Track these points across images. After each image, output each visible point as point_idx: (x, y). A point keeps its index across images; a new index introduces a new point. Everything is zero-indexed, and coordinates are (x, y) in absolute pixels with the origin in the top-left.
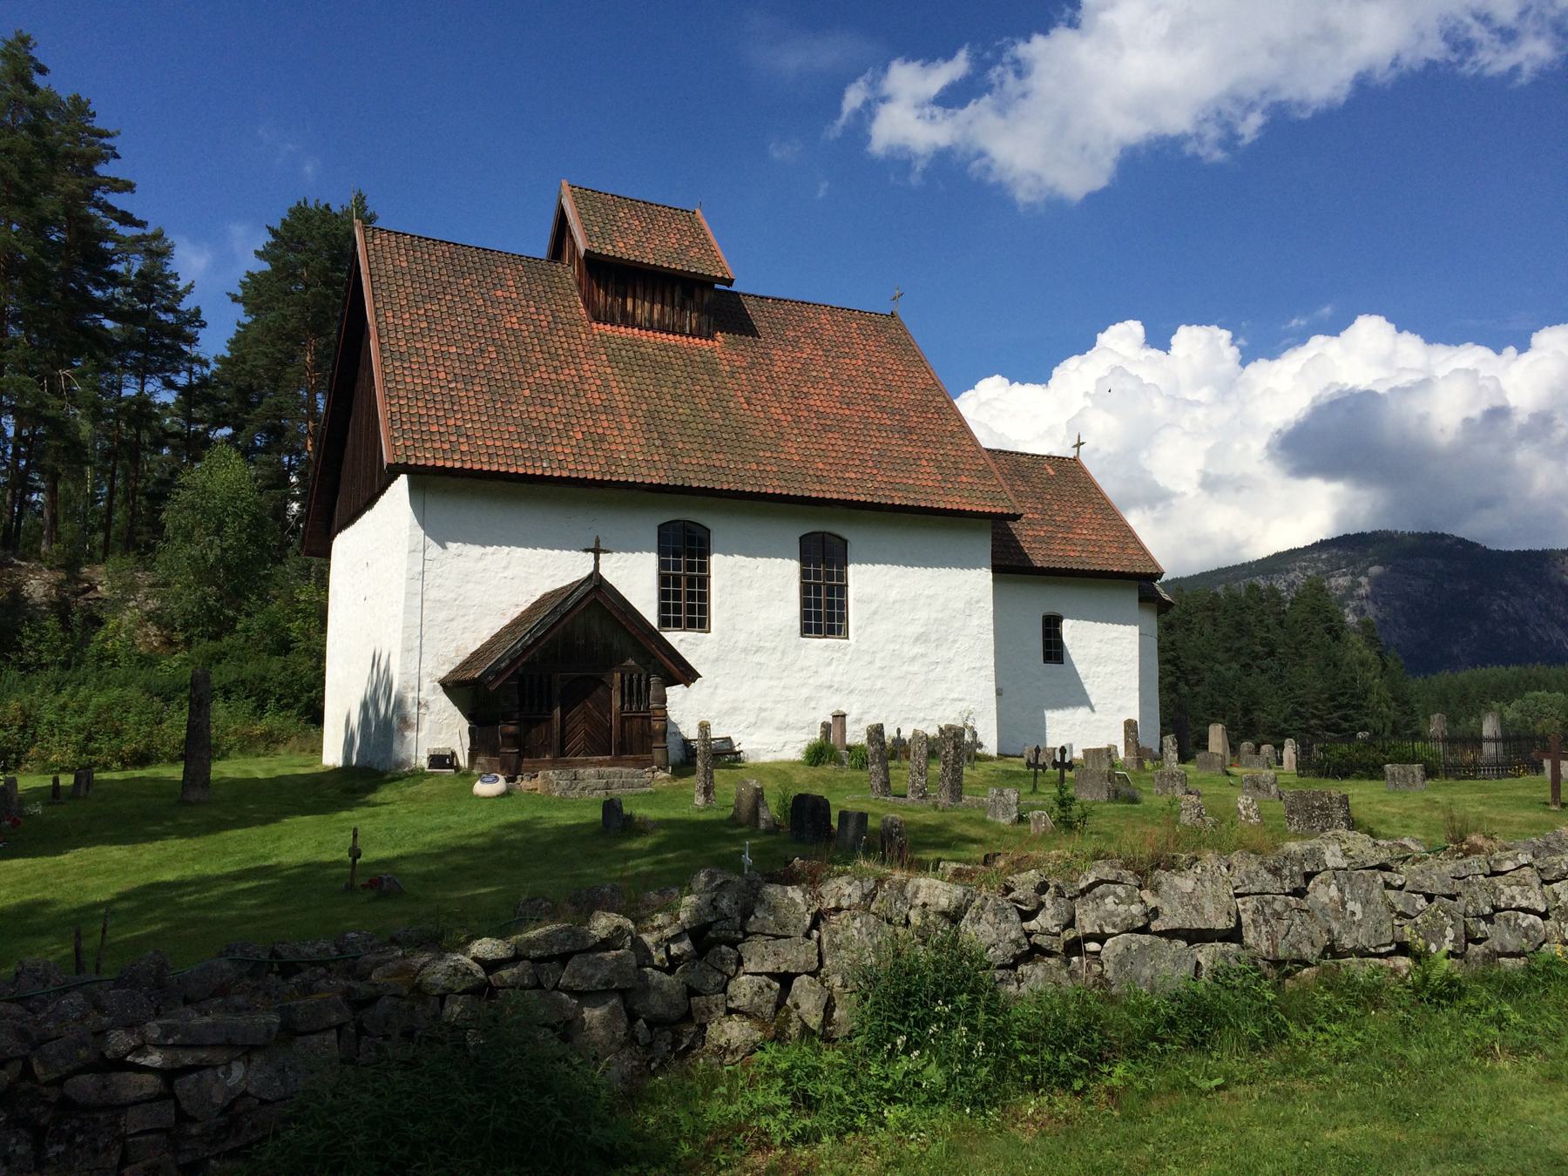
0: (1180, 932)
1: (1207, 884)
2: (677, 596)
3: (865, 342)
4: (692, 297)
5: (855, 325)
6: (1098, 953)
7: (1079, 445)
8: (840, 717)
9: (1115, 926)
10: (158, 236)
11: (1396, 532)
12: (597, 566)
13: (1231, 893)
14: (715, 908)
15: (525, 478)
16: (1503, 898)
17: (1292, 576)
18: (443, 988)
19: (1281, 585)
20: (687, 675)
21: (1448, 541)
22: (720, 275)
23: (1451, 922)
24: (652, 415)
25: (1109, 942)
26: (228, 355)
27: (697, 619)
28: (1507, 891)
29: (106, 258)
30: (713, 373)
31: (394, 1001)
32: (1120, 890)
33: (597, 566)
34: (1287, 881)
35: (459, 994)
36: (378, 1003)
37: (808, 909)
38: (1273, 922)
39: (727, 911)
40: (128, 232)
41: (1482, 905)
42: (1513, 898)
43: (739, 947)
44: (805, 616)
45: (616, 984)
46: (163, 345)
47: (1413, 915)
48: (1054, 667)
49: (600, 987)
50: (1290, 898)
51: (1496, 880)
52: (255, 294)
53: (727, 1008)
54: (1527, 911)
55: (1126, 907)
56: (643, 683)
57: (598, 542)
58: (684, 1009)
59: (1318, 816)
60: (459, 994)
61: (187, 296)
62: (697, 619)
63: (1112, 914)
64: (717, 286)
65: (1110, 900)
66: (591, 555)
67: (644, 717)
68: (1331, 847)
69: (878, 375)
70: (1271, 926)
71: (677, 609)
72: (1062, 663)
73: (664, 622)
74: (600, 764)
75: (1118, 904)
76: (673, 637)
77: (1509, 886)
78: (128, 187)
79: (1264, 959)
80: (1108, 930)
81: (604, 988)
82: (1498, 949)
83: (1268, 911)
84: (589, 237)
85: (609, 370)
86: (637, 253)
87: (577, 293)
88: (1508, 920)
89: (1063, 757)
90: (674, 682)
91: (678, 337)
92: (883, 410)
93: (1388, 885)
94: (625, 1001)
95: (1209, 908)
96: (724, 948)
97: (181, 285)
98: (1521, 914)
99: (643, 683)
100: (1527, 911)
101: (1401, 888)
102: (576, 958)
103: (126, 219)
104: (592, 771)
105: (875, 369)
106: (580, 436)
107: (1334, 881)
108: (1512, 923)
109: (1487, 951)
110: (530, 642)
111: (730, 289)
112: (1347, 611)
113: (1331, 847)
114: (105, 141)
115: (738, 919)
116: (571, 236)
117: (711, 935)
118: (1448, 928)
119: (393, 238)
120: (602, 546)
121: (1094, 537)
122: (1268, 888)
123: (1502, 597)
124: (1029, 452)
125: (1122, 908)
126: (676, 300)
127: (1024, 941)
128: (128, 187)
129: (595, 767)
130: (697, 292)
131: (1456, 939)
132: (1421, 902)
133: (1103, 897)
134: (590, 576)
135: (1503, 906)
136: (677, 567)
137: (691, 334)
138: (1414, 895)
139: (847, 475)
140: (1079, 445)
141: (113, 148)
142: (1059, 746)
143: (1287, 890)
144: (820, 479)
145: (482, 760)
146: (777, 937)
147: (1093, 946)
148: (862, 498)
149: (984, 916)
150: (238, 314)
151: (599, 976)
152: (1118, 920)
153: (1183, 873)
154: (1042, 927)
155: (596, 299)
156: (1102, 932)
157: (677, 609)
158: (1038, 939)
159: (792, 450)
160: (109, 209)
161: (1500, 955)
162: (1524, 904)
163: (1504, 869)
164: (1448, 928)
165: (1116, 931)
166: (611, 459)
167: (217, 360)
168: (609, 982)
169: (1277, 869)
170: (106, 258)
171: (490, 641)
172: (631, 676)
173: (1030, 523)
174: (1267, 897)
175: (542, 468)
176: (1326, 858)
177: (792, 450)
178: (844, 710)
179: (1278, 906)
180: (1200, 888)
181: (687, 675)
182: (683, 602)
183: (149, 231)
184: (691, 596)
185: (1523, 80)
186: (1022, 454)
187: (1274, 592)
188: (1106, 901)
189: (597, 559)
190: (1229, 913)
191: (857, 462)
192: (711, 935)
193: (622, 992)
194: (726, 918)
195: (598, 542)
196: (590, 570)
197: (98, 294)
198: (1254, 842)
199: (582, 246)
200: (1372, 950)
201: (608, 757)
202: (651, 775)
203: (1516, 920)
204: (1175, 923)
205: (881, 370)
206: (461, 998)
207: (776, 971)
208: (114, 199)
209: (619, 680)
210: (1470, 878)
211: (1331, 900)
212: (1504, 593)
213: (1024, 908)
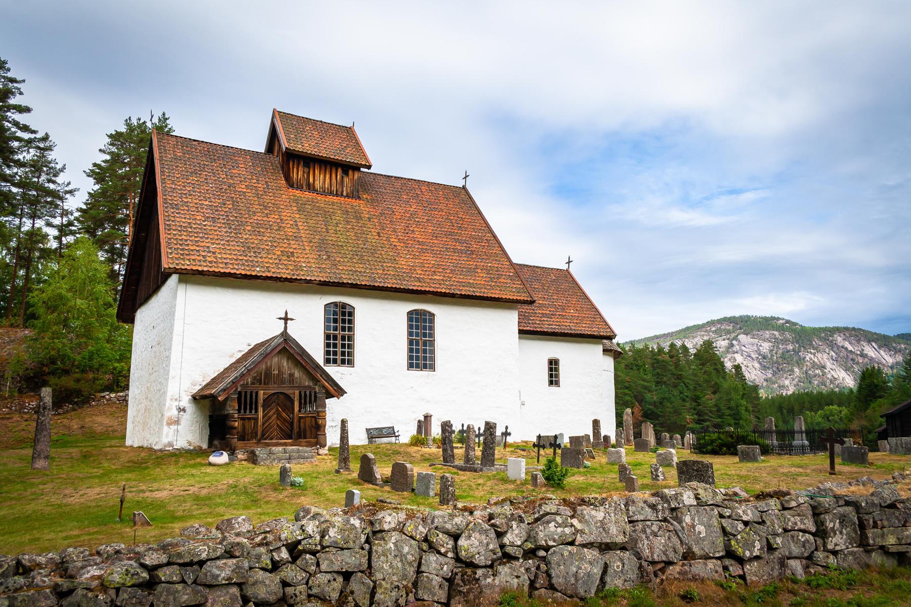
0: (595, 545)
1: (612, 515)
2: (335, 346)
3: (447, 202)
5: (441, 193)
6: (545, 557)
7: (569, 262)
8: (427, 417)
9: (554, 541)
10: (46, 138)
11: (752, 316)
12: (286, 328)
13: (626, 520)
14: (303, 531)
15: (245, 277)
16: (790, 524)
17: (696, 339)
18: (118, 583)
19: (689, 345)
20: (339, 392)
21: (781, 321)
22: (363, 163)
23: (758, 538)
24: (323, 241)
25: (552, 550)
26: (84, 207)
27: (347, 360)
28: (792, 519)
29: (13, 151)
30: (359, 218)
31: (85, 592)
32: (558, 518)
33: (286, 328)
34: (660, 513)
35: (129, 587)
36: (74, 594)
37: (363, 531)
38: (651, 537)
39: (311, 533)
40: (26, 136)
41: (777, 528)
42: (796, 524)
43: (317, 555)
44: (410, 358)
45: (235, 580)
46: (46, 202)
47: (736, 533)
48: (554, 388)
49: (224, 582)
50: (663, 523)
51: (786, 512)
52: (98, 174)
53: (308, 594)
54: (804, 531)
55: (562, 529)
56: (313, 397)
57: (286, 313)
58: (280, 595)
59: (695, 476)
60: (129, 587)
61: (62, 173)
62: (347, 360)
63: (553, 533)
64: (362, 169)
65: (553, 524)
66: (289, 322)
68: (687, 492)
69: (454, 221)
70: (650, 540)
71: (335, 353)
72: (432, 368)
73: (327, 361)
74: (285, 444)
75: (557, 527)
76: (331, 370)
77: (793, 516)
78: (27, 110)
79: (646, 561)
80: (551, 543)
81: (227, 582)
82: (787, 554)
83: (648, 531)
84: (288, 140)
85: (298, 216)
86: (316, 150)
87: (281, 172)
88: (792, 537)
89: (555, 441)
90: (330, 396)
91: (339, 198)
92: (457, 240)
93: (721, 516)
94: (241, 590)
95: (614, 530)
96: (308, 556)
97: (59, 167)
98: (801, 534)
99: (313, 397)
100: (804, 531)
101: (729, 517)
102: (208, 563)
103: (25, 128)
104: (280, 448)
105: (452, 218)
106: (279, 253)
107: (689, 513)
108: (795, 539)
109: (780, 556)
110: (245, 372)
111: (369, 171)
112: (726, 360)
113: (687, 492)
114: (15, 85)
115: (318, 538)
116: (278, 141)
117: (300, 547)
118: (757, 542)
119: (334, 188)
120: (283, 316)
121: (577, 315)
122: (649, 518)
123: (811, 353)
124: (540, 266)
125: (559, 530)
126: (338, 177)
127: (499, 550)
128: (27, 110)
129: (282, 446)
130: (350, 172)
131: (762, 548)
132: (740, 526)
133: (548, 522)
134: (282, 334)
135: (790, 528)
137: (348, 196)
138: (736, 522)
139: (435, 277)
140: (569, 262)
141: (19, 89)
142: (479, 425)
143: (660, 518)
144: (419, 280)
145: (216, 442)
146: (342, 549)
147: (542, 553)
148: (443, 291)
149: (473, 535)
150: (91, 185)
151: (223, 575)
152: (556, 537)
153: (598, 508)
154: (510, 542)
155: (291, 175)
156: (547, 545)
157: (335, 353)
158: (509, 550)
159: (404, 262)
160: (16, 124)
161: (789, 558)
162: (802, 527)
163: (791, 506)
164: (757, 542)
165: (555, 544)
166: (298, 268)
167: (78, 210)
168: (229, 579)
169: (654, 505)
170: (13, 151)
171: (223, 372)
172: (305, 392)
173: (541, 306)
174: (648, 523)
175: (257, 271)
176: (684, 499)
177: (404, 262)
178: (431, 412)
179: (655, 528)
180: (608, 517)
181: (339, 392)
182: (339, 349)
183: (39, 136)
184: (343, 346)
186: (537, 267)
187: (685, 348)
188: (550, 525)
189: (286, 324)
190: (624, 533)
191: (441, 270)
192: (300, 547)
193: (240, 585)
194: (311, 537)
195: (286, 313)
197: (8, 172)
199: (285, 144)
200: (711, 555)
201: (290, 441)
203: (798, 537)
204: (591, 539)
205: (456, 218)
206: (129, 589)
207: (340, 570)
208: (17, 117)
209: (298, 395)
210: (770, 512)
212: (813, 351)
213: (499, 530)
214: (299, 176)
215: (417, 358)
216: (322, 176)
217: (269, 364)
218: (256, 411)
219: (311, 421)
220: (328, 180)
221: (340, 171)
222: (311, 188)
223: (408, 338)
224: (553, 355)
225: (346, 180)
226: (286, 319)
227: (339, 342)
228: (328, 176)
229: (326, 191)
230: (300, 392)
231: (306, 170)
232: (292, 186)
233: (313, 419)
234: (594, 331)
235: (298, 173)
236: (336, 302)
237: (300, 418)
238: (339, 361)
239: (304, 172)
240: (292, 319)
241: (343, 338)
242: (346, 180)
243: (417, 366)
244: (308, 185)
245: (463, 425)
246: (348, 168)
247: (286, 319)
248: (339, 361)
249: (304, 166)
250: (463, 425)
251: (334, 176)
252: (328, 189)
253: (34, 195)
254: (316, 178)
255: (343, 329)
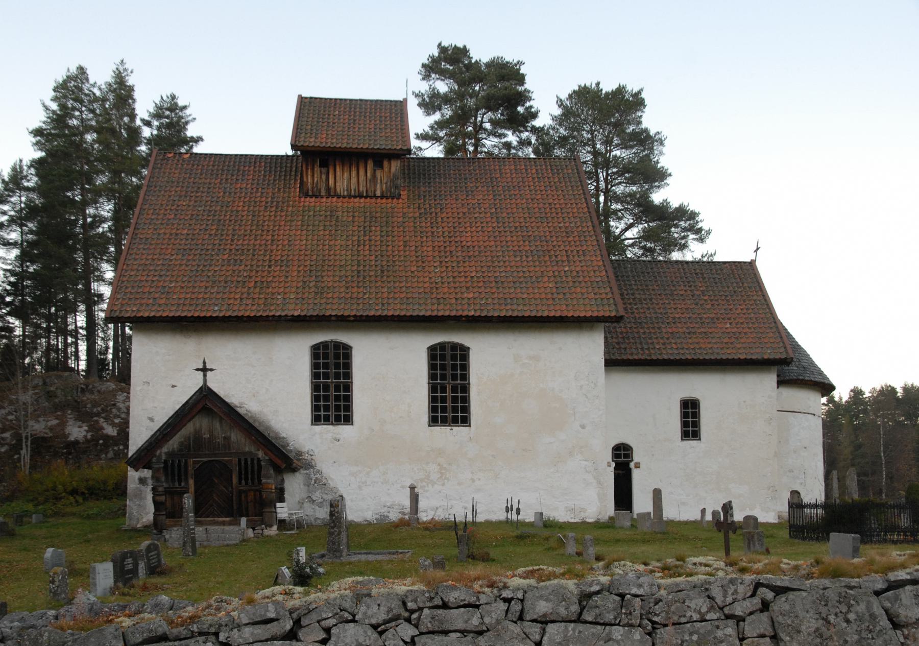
4: (381, 167)
12: (205, 381)
33: (205, 381)
44: (433, 409)
57: (204, 363)
66: (201, 373)
67: (257, 490)
71: (444, 409)
74: (223, 523)
120: (201, 366)
130: (386, 164)
136: (326, 376)
137: (382, 197)
155: (305, 179)
157: (444, 409)
185: (198, 149)
189: (205, 376)
195: (204, 363)
196: (201, 384)
198: (783, 599)
202: (261, 532)
211: (614, 610)
214: (315, 181)
215: (327, 408)
216: (345, 175)
217: (198, 425)
218: (187, 483)
219: (255, 495)
220: (354, 180)
221: (370, 165)
222: (331, 193)
223: (429, 383)
224: (688, 394)
225: (379, 174)
226: (204, 370)
227: (332, 393)
228: (354, 173)
229: (353, 192)
230: (240, 460)
231: (324, 170)
232: (307, 195)
233: (258, 493)
234: (768, 354)
235: (313, 176)
236: (326, 342)
237: (240, 493)
238: (332, 418)
239: (321, 172)
240: (211, 370)
241: (337, 388)
242: (379, 174)
243: (327, 420)
244: (328, 189)
245: (703, 511)
246: (379, 158)
247: (204, 370)
248: (332, 418)
249: (321, 166)
250: (703, 511)
251: (362, 172)
252: (355, 190)
253: (615, 255)
254: (338, 178)
255: (337, 376)
